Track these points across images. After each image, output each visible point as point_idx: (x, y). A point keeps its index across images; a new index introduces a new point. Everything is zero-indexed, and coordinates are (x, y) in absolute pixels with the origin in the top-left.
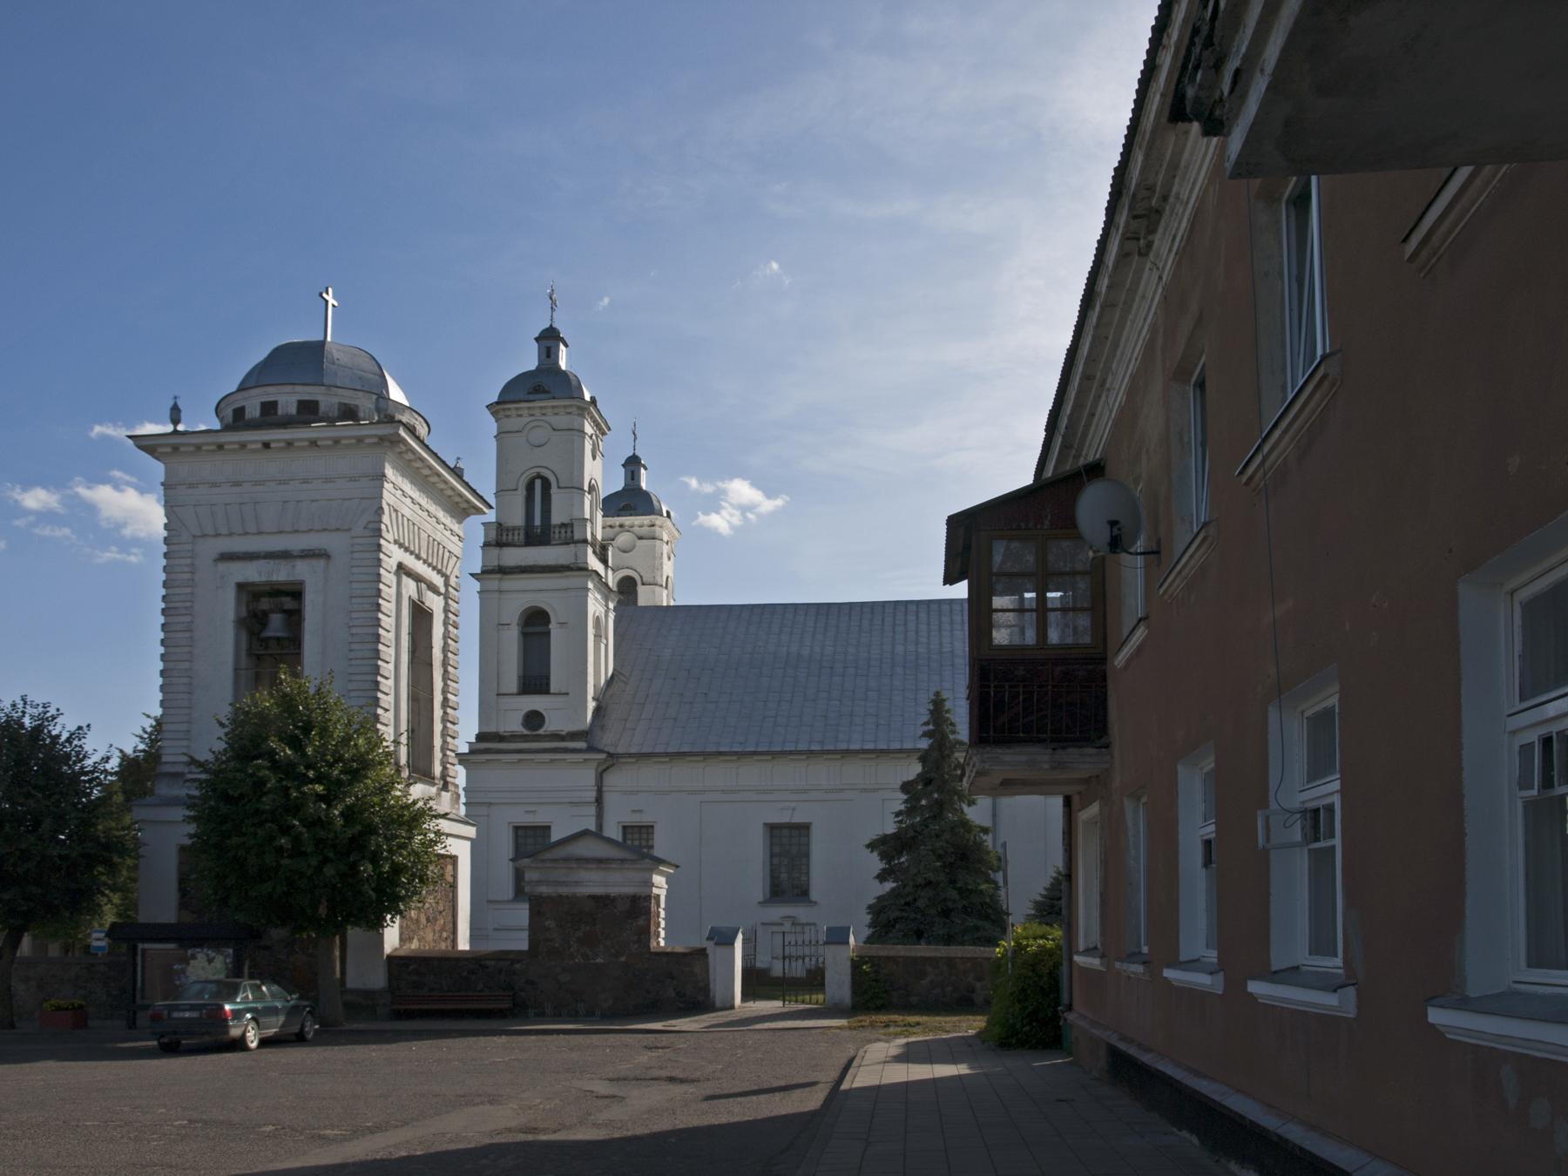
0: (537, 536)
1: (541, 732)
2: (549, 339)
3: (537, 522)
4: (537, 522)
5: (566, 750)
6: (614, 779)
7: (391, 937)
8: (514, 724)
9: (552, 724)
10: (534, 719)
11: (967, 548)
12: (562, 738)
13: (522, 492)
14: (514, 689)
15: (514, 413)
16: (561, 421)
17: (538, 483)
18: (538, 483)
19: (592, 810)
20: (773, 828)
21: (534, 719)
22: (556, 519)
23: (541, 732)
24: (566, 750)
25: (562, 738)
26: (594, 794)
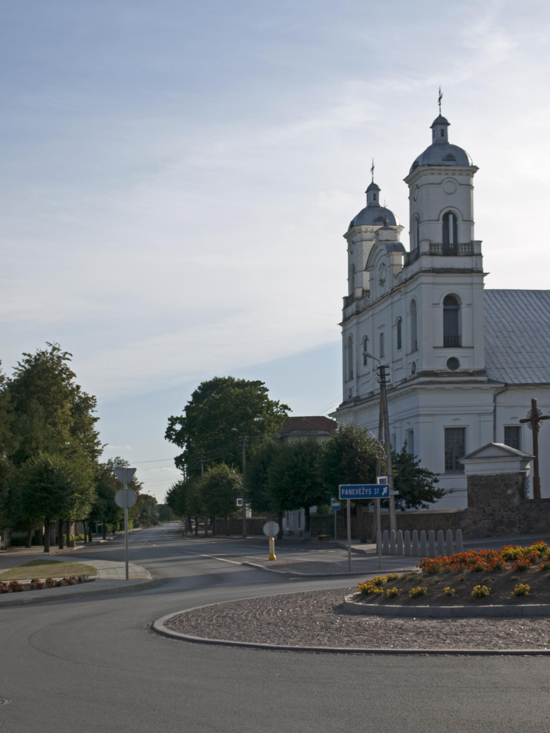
0: (450, 249)
1: (458, 370)
2: (440, 125)
3: (451, 241)
4: (451, 241)
5: (476, 382)
6: (501, 399)
7: (5, 456)
8: (441, 365)
9: (464, 366)
10: (453, 362)
11: (353, 278)
12: (471, 374)
13: (440, 224)
14: (441, 344)
15: (443, 172)
16: (461, 179)
17: (451, 217)
18: (451, 217)
19: (491, 418)
20: (448, 430)
21: (453, 362)
22: (462, 240)
23: (458, 370)
24: (476, 382)
25: (471, 374)
26: (493, 408)
